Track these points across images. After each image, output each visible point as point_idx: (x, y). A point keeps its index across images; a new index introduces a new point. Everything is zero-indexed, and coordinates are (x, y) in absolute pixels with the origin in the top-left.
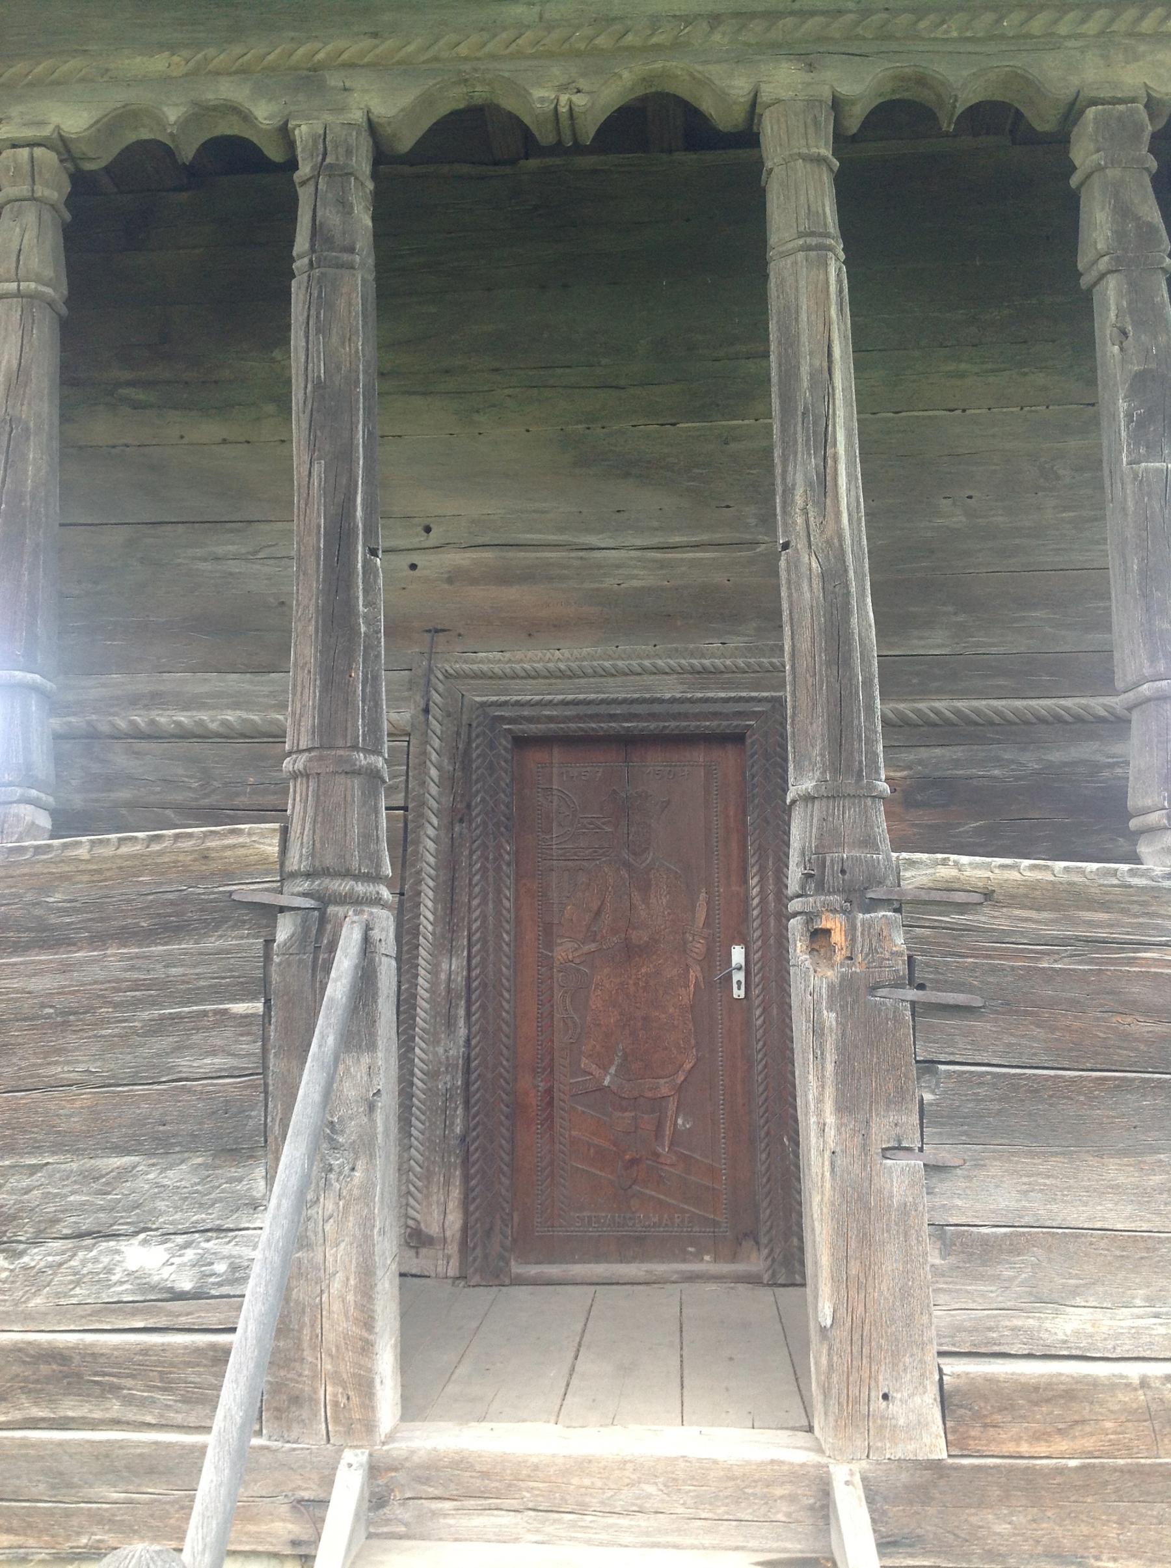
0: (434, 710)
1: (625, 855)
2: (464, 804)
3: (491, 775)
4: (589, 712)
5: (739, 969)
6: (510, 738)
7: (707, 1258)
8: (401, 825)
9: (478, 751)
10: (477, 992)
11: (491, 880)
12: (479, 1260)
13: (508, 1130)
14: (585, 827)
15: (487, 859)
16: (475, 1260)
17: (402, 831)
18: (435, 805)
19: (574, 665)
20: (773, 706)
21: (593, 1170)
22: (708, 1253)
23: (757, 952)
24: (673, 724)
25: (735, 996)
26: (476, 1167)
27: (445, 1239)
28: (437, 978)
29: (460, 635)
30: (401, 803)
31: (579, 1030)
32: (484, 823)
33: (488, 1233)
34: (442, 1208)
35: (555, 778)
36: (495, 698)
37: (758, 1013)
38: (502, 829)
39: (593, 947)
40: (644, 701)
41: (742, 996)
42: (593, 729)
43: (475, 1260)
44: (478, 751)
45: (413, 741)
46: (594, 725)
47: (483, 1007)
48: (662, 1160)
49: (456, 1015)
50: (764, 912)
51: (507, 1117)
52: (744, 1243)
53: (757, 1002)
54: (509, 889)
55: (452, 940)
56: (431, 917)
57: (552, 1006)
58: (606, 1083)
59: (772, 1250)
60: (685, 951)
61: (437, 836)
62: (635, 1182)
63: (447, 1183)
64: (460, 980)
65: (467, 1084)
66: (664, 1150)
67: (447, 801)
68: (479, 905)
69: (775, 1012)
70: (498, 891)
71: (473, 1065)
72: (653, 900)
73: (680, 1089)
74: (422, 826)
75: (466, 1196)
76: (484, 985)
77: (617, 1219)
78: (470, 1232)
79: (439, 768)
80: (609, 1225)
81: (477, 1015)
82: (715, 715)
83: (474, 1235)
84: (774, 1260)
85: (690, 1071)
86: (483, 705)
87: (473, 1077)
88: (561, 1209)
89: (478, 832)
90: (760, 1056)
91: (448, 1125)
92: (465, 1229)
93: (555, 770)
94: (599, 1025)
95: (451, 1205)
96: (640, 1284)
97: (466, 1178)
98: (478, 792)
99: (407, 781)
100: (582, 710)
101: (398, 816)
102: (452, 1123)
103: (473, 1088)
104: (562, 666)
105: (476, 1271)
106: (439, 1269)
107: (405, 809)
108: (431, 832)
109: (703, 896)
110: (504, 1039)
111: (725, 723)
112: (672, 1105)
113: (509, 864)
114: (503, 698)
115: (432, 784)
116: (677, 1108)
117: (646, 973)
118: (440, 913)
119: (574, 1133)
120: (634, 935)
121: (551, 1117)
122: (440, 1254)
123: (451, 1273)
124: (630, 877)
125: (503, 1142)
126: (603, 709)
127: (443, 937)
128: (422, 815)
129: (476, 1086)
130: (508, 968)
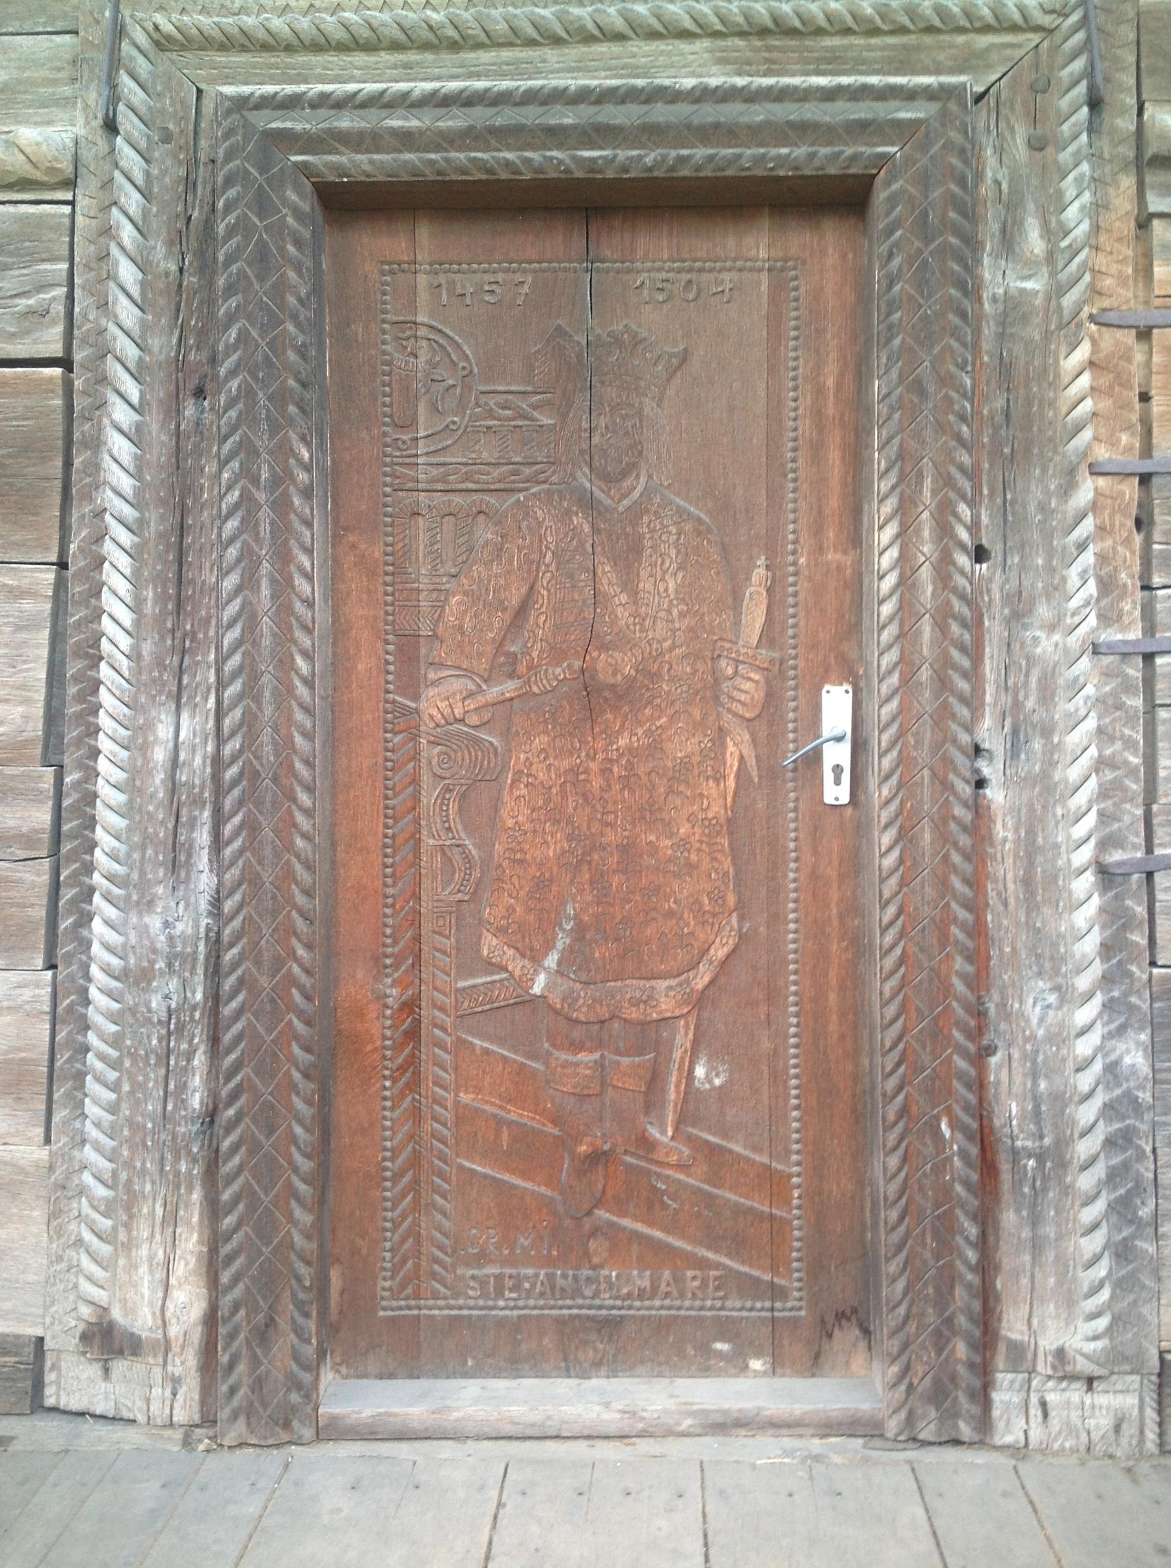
0: (127, 122)
1: (583, 479)
2: (204, 355)
3: (261, 278)
4: (499, 121)
5: (839, 739)
6: (309, 188)
7: (756, 1364)
8: (58, 402)
9: (231, 219)
10: (236, 792)
11: (265, 530)
12: (242, 1392)
13: (309, 1102)
14: (491, 415)
15: (255, 481)
16: (233, 1391)
17: (59, 417)
18: (131, 352)
20: (944, 112)
21: (506, 1177)
22: (758, 1355)
24: (700, 153)
25: (829, 799)
26: (236, 1187)
28: (146, 759)
30: (56, 349)
31: (476, 874)
32: (248, 394)
33: (264, 1333)
34: (160, 1275)
35: (423, 297)
36: (269, 89)
37: (887, 839)
38: (292, 409)
39: (509, 688)
41: (845, 799)
42: (507, 164)
43: (233, 1391)
44: (231, 219)
45: (82, 203)
46: (510, 156)
47: (250, 827)
48: (660, 1156)
50: (907, 611)
51: (306, 1076)
52: (837, 1333)
53: (885, 816)
54: (309, 551)
55: (181, 672)
56: (126, 618)
57: (417, 821)
58: (537, 989)
59: (907, 1369)
60: (716, 698)
61: (139, 427)
62: (599, 1203)
63: (172, 1219)
64: (198, 764)
65: (215, 999)
66: (662, 1134)
67: (162, 344)
68: (238, 590)
69: (927, 836)
70: (283, 557)
71: (229, 956)
72: (646, 585)
73: (700, 1001)
74: (102, 405)
75: (213, 1250)
76: (251, 775)
77: (560, 1282)
78: (222, 1331)
79: (142, 264)
80: (542, 1294)
81: (237, 844)
82: (803, 130)
83: (232, 1336)
84: (910, 1388)
85: (724, 963)
86: (241, 103)
87: (228, 984)
88: (436, 1261)
89: (233, 413)
90: (889, 939)
91: (174, 1093)
92: (211, 1319)
93: (422, 280)
94: (521, 862)
95: (180, 1269)
96: (607, 1437)
97: (214, 1209)
98: (231, 318)
99: (70, 297)
100: (480, 116)
101: (51, 379)
102: (183, 1087)
103: (227, 1010)
105: (235, 1416)
106: (155, 1407)
107: (65, 363)
108: (122, 414)
109: (759, 573)
110: (300, 899)
111: (824, 151)
112: (683, 1039)
113: (307, 493)
114: (290, 89)
115: (123, 301)
116: (696, 1043)
117: (630, 750)
118: (149, 608)
119: (465, 1098)
120: (602, 661)
121: (413, 1062)
122: (157, 1372)
123: (180, 1416)
124: (595, 530)
125: (298, 1130)
126: (530, 116)
127: (160, 664)
128: (103, 379)
129: (234, 1005)
130: (308, 736)
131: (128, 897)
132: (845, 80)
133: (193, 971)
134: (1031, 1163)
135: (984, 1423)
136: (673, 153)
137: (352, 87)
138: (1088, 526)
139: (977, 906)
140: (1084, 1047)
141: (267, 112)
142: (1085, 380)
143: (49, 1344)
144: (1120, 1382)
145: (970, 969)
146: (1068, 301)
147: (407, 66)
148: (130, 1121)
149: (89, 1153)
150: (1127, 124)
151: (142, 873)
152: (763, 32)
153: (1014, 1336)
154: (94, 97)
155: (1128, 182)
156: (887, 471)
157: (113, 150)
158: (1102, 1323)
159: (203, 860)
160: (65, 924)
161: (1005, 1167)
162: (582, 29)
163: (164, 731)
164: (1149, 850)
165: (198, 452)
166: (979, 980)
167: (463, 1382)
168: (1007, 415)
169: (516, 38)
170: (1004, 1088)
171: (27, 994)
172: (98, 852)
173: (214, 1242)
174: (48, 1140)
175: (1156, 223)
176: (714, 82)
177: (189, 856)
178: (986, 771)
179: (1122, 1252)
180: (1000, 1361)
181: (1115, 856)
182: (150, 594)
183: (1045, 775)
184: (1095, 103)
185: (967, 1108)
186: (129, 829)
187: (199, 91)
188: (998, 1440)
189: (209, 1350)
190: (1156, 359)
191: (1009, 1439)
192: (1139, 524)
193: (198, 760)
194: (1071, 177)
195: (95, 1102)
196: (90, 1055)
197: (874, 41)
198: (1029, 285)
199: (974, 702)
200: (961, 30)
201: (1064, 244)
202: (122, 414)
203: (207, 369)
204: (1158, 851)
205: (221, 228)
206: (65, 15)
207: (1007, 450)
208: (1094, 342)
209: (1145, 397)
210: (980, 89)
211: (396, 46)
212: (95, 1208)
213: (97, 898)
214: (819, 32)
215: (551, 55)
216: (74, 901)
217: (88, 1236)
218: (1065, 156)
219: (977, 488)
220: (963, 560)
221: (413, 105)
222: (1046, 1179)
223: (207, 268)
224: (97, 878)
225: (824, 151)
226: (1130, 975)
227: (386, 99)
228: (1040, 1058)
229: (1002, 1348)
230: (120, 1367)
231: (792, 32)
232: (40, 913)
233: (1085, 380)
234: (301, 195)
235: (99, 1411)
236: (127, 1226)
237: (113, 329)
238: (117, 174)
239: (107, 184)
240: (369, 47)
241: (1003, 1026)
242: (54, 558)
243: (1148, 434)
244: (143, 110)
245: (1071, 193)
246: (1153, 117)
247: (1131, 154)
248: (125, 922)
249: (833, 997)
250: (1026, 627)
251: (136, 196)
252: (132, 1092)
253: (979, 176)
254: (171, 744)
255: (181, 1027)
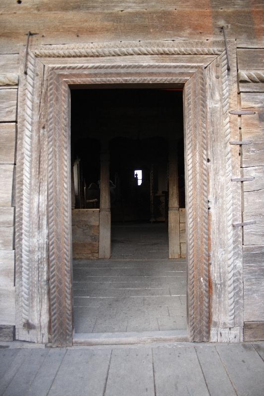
0: (29, 72)
2: (45, 120)
6: (67, 86)
9: (51, 92)
15: (55, 146)
17: (14, 134)
18: (30, 120)
19: (100, 50)
23: (190, 191)
27: (41, 326)
29: (43, 36)
30: (14, 119)
34: (39, 313)
40: (135, 67)
44: (51, 92)
49: (42, 223)
63: (41, 301)
64: (43, 207)
65: (48, 256)
67: (36, 118)
75: (50, 308)
86: (53, 68)
87: (51, 253)
92: (50, 322)
97: (49, 300)
98: (51, 112)
99: (17, 108)
102: (42, 275)
104: (94, 50)
106: (39, 339)
107: (16, 122)
111: (174, 78)
114: (63, 65)
118: (33, 174)
128: (23, 125)
131: (29, 235)
132: (178, 64)
133: (43, 250)
134: (219, 286)
135: (209, 338)
136: (143, 78)
137: (76, 65)
138: (229, 156)
139: (208, 234)
140: (230, 262)
141: (59, 70)
142: (228, 125)
143: (16, 327)
144: (235, 329)
145: (207, 247)
146: (225, 109)
147: (87, 60)
148: (32, 282)
149: (23, 288)
150: (235, 74)
151: (32, 230)
152: (162, 54)
153: (215, 320)
154: (22, 67)
155: (236, 85)
156: (189, 143)
157: (26, 78)
158: (232, 317)
159: (45, 227)
160: (17, 240)
161: (213, 287)
162: (124, 53)
163: (36, 200)
164: (242, 221)
165: (44, 140)
166: (209, 250)
167: (109, 230)
168: (213, 132)
169: (110, 55)
170: (213, 271)
171: (9, 255)
172: (23, 225)
173: (50, 306)
174: (15, 285)
175: (241, 93)
176: (151, 64)
177: (42, 226)
178: (210, 206)
179: (237, 302)
180: (212, 326)
181: (236, 223)
182: (33, 170)
183: (222, 207)
184: (229, 69)
185: (206, 275)
186: (30, 220)
187: (44, 66)
188: (212, 341)
189: (50, 328)
190: (242, 121)
191: (214, 341)
192: (240, 154)
193: (43, 205)
194: (224, 84)
195: (24, 278)
196: (23, 268)
197: (184, 56)
198: (217, 105)
199: (208, 191)
200: (202, 54)
201: (223, 97)
202: (27, 133)
203: (45, 123)
204: (244, 222)
205: (49, 94)
206: (16, 50)
207: (213, 139)
208: (230, 117)
209: (240, 128)
210: (205, 66)
211: (85, 56)
212: (25, 300)
213: (23, 235)
214: (173, 54)
215: (118, 58)
216: (19, 236)
217: (24, 305)
218: (223, 80)
219: (207, 147)
220: (205, 162)
221: (89, 69)
222: (222, 289)
223: (45, 102)
224: (23, 231)
225: (174, 78)
226: (239, 247)
227: (83, 67)
228: (221, 265)
229: (213, 323)
230: (32, 331)
231: (167, 54)
232: (11, 238)
233: (228, 125)
234: (66, 87)
235: (27, 340)
236: (32, 303)
237: (26, 115)
238: (27, 83)
239: (25, 85)
240: (80, 56)
241: (214, 259)
242: (13, 163)
243: (241, 136)
244: (33, 70)
245: (224, 87)
246: (240, 73)
247: (236, 80)
248: (29, 240)
249: (58, 176)
250: (218, 176)
251: (31, 87)
252: (32, 276)
253: (206, 84)
254: (38, 203)
255: (41, 263)
